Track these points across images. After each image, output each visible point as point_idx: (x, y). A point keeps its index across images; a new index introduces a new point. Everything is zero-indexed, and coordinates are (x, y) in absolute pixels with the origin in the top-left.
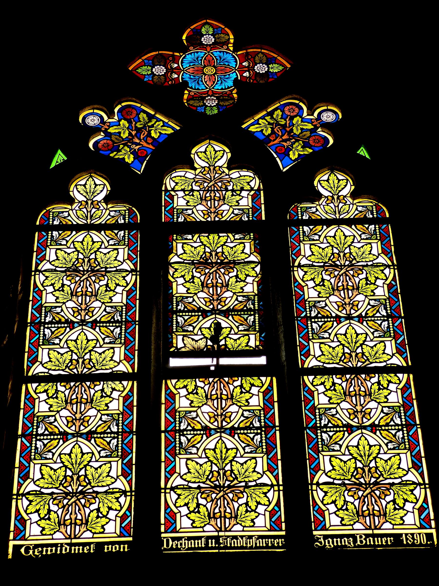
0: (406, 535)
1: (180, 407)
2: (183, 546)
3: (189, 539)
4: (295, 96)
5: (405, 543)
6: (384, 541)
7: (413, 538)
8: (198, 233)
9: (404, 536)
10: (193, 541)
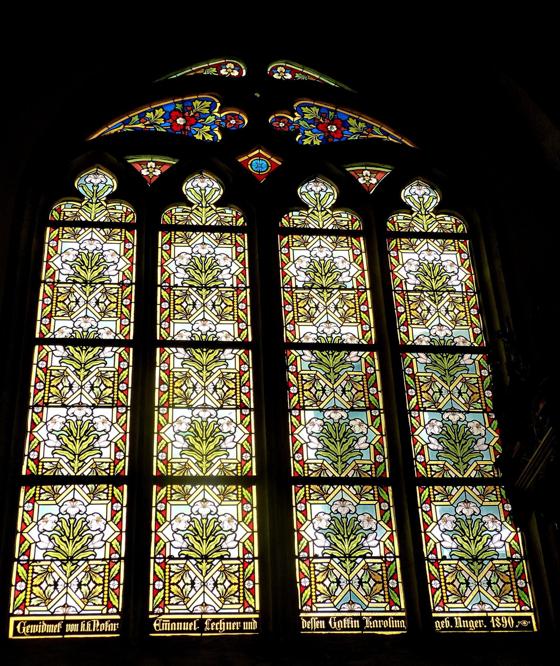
0: (495, 617)
1: (43, 458)
2: (221, 629)
3: (226, 620)
4: (216, 94)
5: (494, 626)
6: (190, 627)
7: (501, 621)
8: (469, 353)
9: (493, 618)
10: (174, 624)
